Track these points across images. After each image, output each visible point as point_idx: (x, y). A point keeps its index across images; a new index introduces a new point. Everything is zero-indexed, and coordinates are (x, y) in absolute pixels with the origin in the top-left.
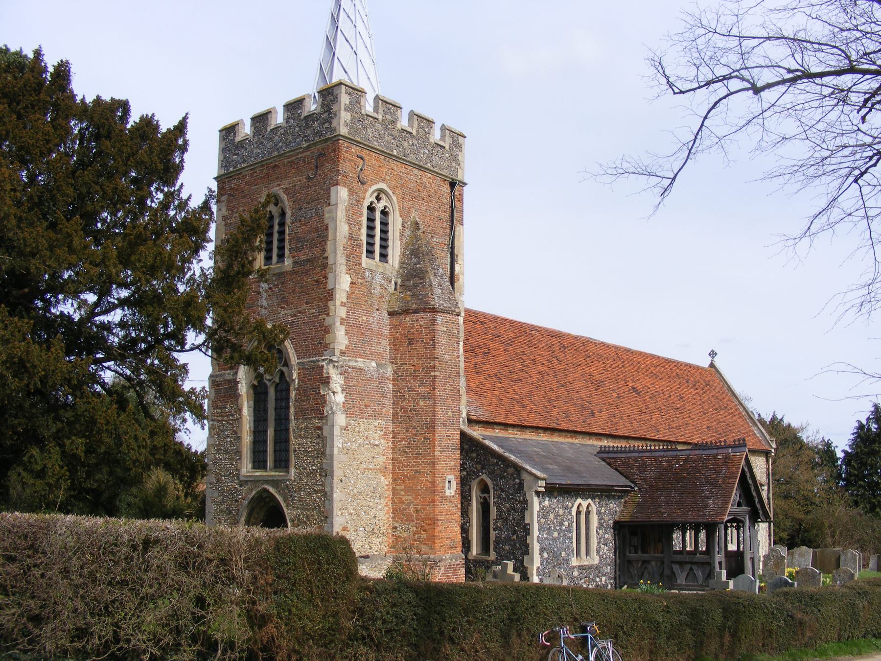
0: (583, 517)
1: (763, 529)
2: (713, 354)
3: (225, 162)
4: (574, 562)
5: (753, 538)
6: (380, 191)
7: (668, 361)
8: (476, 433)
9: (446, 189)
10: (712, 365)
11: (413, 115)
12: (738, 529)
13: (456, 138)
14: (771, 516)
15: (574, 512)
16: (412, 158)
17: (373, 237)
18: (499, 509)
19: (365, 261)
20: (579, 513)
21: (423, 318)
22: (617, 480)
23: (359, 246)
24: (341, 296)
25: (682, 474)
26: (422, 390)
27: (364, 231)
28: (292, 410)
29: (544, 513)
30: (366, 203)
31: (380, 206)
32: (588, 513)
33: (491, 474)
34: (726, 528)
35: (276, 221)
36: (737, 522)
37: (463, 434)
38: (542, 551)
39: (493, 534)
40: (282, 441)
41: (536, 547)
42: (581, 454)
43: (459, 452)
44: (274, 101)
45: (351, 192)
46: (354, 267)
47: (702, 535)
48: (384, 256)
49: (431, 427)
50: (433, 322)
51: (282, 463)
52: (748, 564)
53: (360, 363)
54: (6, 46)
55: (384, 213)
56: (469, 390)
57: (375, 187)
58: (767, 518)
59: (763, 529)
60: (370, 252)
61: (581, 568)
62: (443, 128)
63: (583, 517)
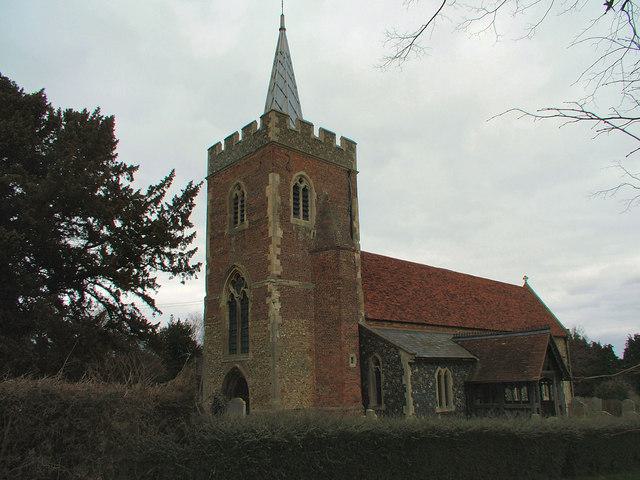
0: (443, 379)
1: (566, 384)
2: (525, 278)
3: (211, 168)
4: (438, 410)
5: (560, 390)
6: (302, 176)
7: (498, 283)
8: (373, 328)
9: (344, 175)
10: (526, 285)
11: (322, 130)
12: (549, 385)
13: (350, 145)
14: (571, 374)
15: (436, 374)
16: (322, 156)
17: (298, 200)
18: (386, 376)
19: (293, 220)
20: (439, 377)
21: (331, 254)
22: (464, 354)
23: (288, 209)
24: (276, 241)
25: (501, 337)
26: (332, 299)
27: (291, 200)
28: (250, 315)
29: (415, 377)
30: (292, 184)
31: (302, 186)
32: (445, 377)
33: (381, 353)
34: (541, 385)
35: (240, 199)
36: (547, 380)
37: (360, 327)
38: (415, 403)
39: (383, 392)
40: (245, 335)
41: (411, 400)
42: (441, 344)
43: (357, 340)
44: (237, 126)
45: (282, 176)
46: (284, 221)
47: (524, 390)
48: (306, 217)
49: (338, 322)
50: (338, 255)
51: (245, 350)
52: (557, 409)
53: (292, 283)
54: (117, 141)
55: (305, 190)
56: (366, 300)
57: (297, 174)
58: (568, 379)
59: (566, 384)
60: (296, 214)
61: (443, 414)
62: (342, 138)
63: (443, 379)
